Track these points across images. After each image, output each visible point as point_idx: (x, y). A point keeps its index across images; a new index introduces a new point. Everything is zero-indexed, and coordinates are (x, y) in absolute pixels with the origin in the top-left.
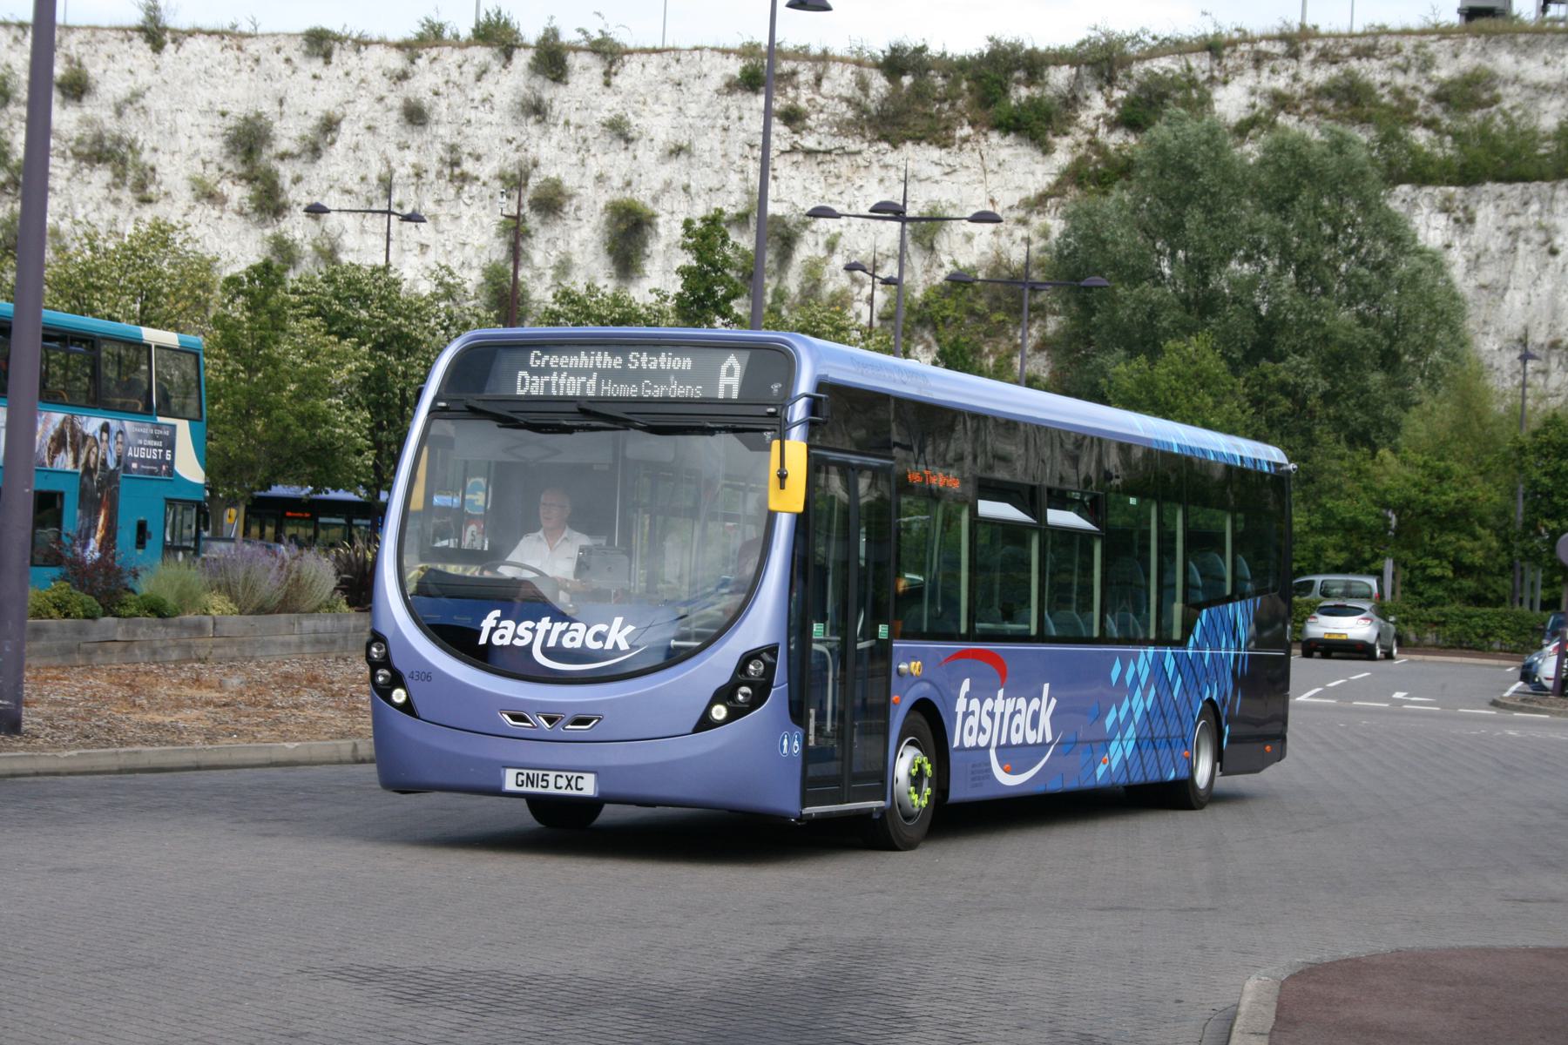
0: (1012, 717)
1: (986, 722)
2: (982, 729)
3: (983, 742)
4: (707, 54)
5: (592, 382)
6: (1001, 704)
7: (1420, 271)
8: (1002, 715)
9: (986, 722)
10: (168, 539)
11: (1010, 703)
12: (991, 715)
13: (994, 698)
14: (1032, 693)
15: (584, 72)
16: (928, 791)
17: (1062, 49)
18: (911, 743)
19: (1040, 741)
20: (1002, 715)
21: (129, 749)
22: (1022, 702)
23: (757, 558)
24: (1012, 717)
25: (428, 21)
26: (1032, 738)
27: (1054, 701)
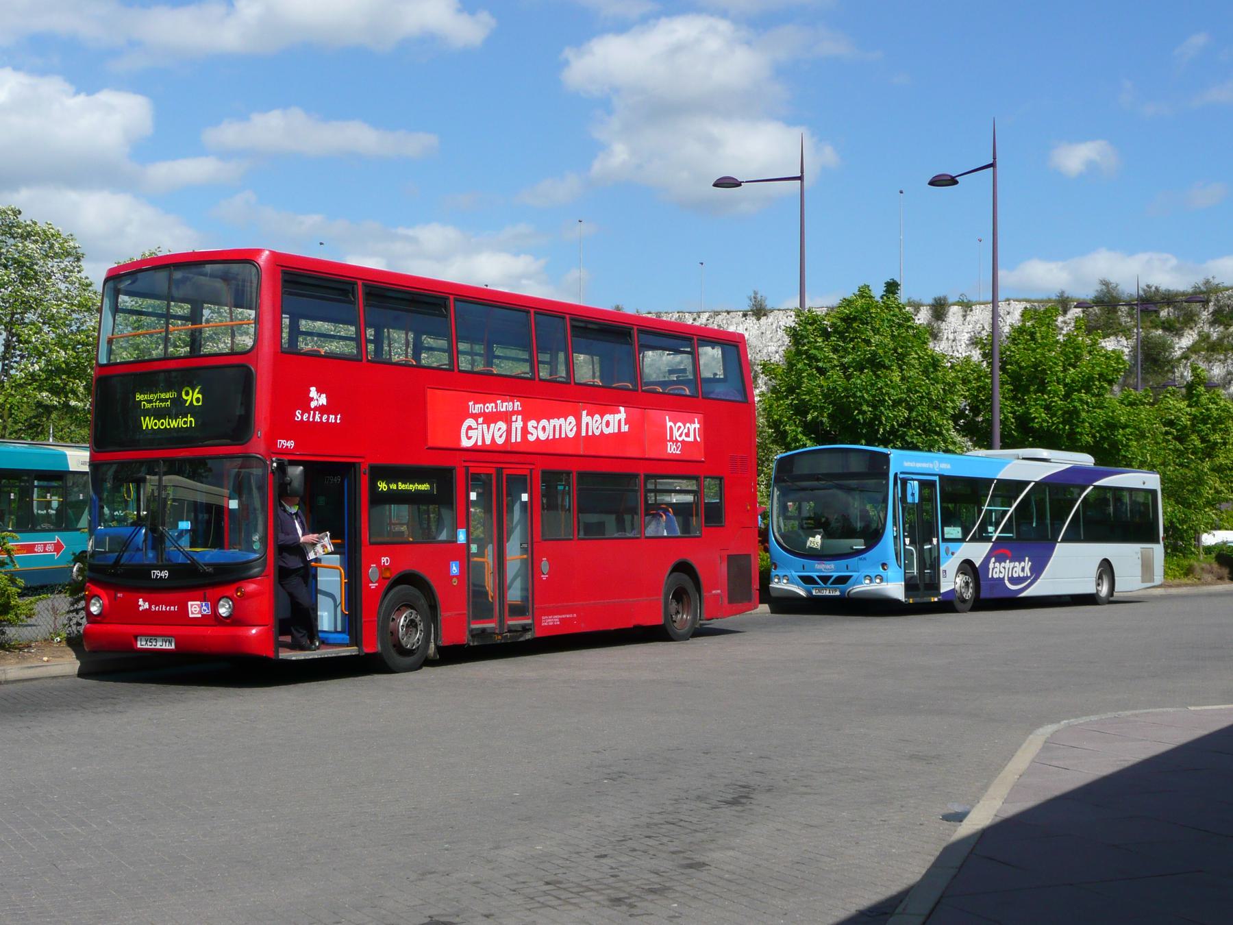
0: (1013, 568)
1: (1002, 570)
2: (1000, 572)
3: (1001, 576)
4: (1012, 301)
5: (518, 424)
6: (1008, 564)
7: (532, 434)
8: (1009, 568)
9: (1002, 570)
10: (663, 506)
11: (1012, 564)
12: (1004, 568)
13: (1005, 562)
14: (1021, 560)
15: (954, 312)
16: (971, 590)
17: (1177, 291)
18: (962, 573)
19: (1025, 575)
20: (1009, 568)
21: (534, 341)
22: (1017, 564)
23: (816, 491)
24: (1013, 568)
25: (844, 299)
26: (1022, 575)
27: (1030, 563)
